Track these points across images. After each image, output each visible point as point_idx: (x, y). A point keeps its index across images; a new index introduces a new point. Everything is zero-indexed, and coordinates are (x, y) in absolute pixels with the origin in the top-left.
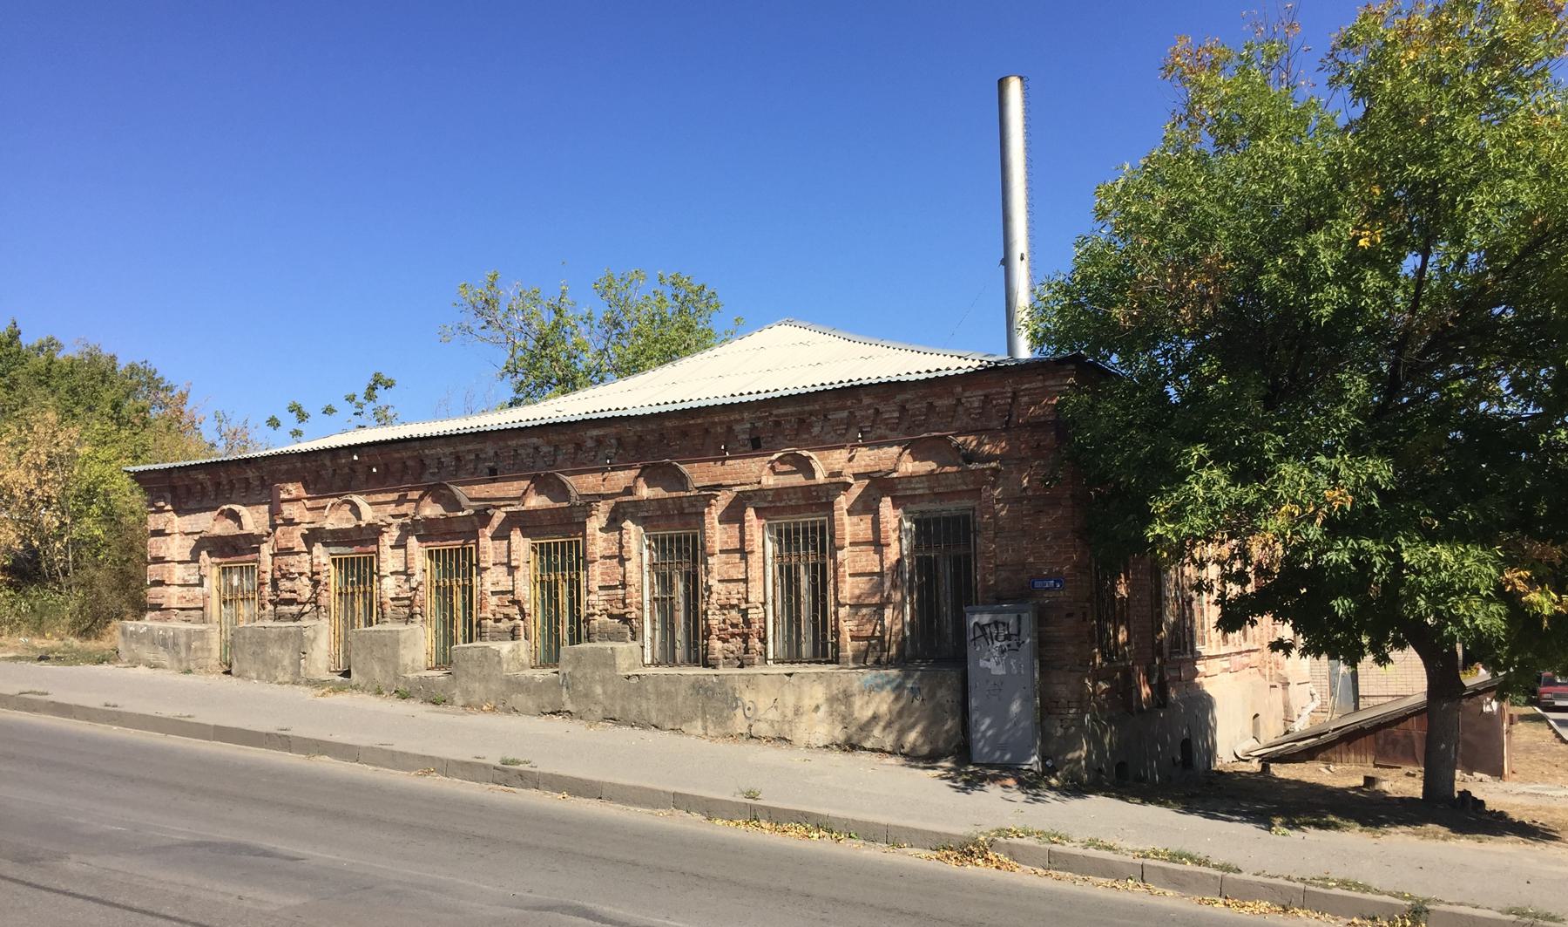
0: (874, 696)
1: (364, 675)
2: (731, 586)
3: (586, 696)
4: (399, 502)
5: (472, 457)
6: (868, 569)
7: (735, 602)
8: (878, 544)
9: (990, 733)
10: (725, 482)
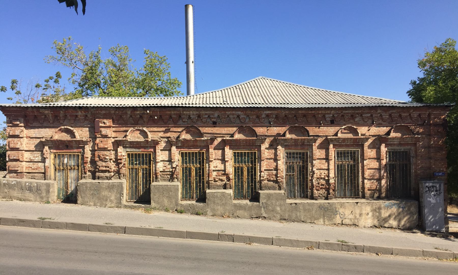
0: (389, 208)
1: (158, 203)
2: (322, 171)
3: (273, 211)
4: (165, 132)
5: (207, 116)
6: (375, 167)
7: (323, 177)
8: (378, 158)
9: (432, 220)
10: (320, 135)
